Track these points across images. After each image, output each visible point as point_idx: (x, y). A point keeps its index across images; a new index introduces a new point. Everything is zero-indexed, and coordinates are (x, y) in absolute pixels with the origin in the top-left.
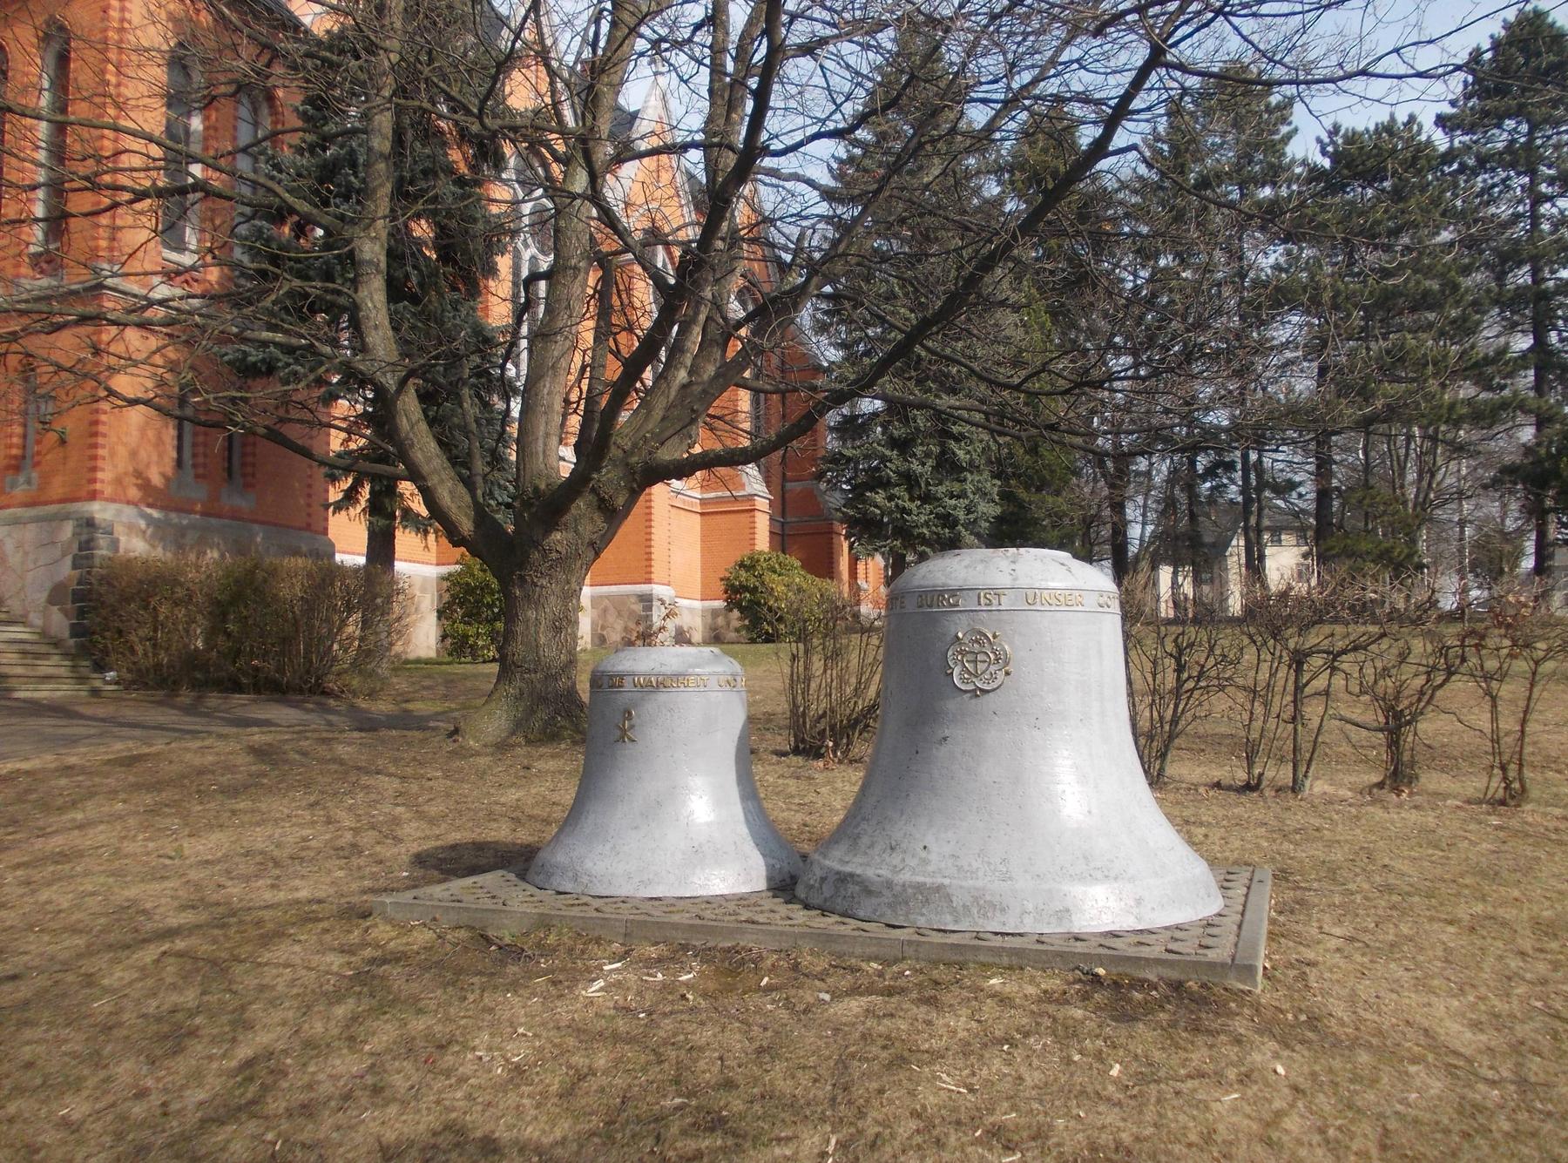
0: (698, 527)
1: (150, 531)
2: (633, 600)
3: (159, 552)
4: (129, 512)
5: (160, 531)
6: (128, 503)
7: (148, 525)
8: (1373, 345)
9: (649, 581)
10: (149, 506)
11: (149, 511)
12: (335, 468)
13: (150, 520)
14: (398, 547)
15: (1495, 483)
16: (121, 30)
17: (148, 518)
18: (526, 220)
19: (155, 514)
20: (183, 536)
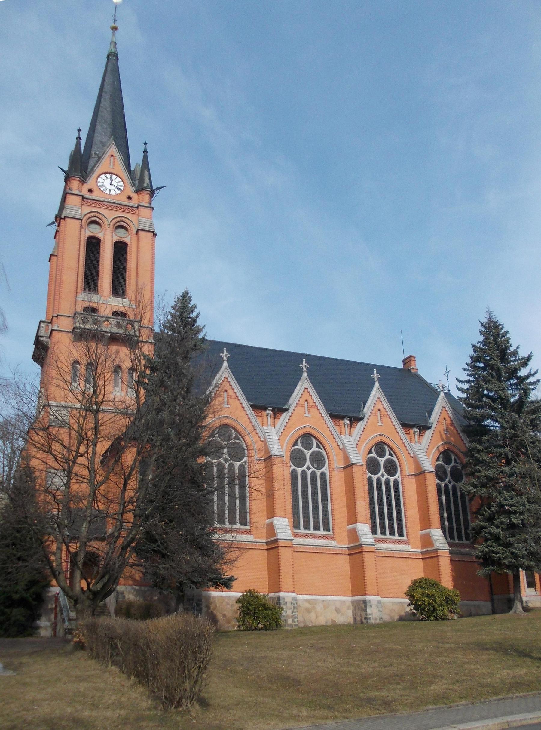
0: (265, 560)
1: (135, 593)
2: (362, 602)
3: (138, 599)
4: (129, 588)
5: (138, 593)
6: (129, 585)
7: (134, 591)
8: (200, 558)
9: (365, 594)
10: (135, 585)
11: (135, 587)
12: (488, 393)
13: (135, 590)
14: (142, 161)
15: (208, 556)
16: (366, 618)
17: (135, 590)
18: (225, 450)
19: (137, 588)
20: (145, 593)
